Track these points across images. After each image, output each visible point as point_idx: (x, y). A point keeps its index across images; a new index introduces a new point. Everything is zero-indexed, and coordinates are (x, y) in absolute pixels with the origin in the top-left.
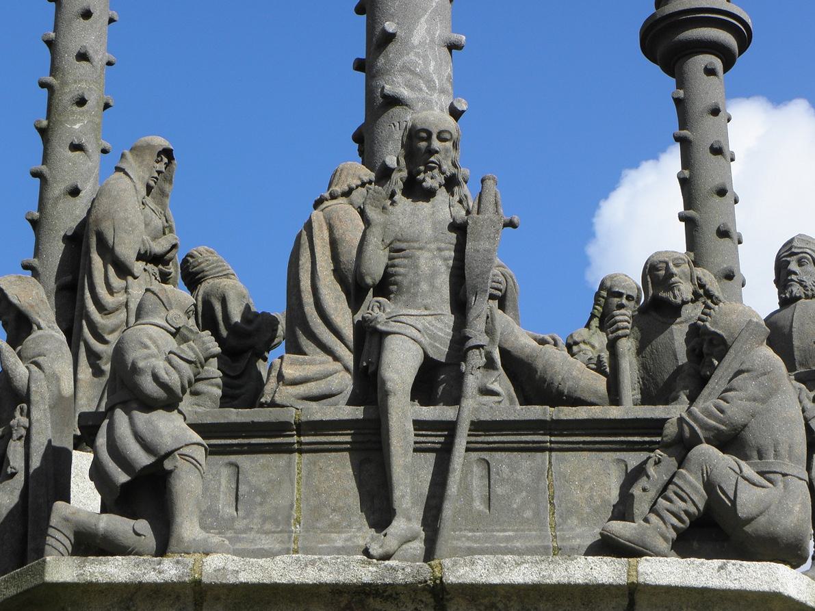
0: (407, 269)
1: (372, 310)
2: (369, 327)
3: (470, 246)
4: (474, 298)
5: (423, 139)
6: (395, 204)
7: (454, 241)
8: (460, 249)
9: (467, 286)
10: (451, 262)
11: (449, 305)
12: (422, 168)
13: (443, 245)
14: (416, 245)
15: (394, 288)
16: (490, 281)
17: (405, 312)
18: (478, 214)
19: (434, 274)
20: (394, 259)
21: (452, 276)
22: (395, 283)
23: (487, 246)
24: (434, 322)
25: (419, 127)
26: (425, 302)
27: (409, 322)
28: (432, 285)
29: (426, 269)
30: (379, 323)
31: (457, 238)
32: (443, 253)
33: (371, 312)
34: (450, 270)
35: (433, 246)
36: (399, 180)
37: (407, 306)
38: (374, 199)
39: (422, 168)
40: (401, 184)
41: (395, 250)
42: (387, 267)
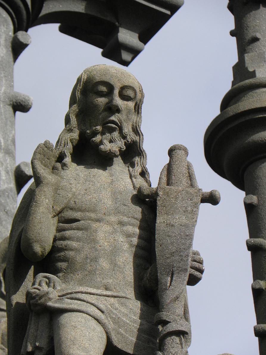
0: (81, 244)
2: (36, 305)
3: (160, 220)
4: (169, 279)
5: (101, 94)
6: (65, 168)
7: (139, 216)
8: (148, 227)
9: (158, 266)
11: (133, 289)
13: (125, 219)
14: (93, 215)
15: (62, 265)
16: (190, 259)
17: (82, 289)
19: (115, 251)
21: (136, 256)
23: (184, 220)
24: (117, 305)
25: (98, 79)
26: (105, 281)
27: (90, 300)
28: (114, 264)
29: (106, 244)
30: (50, 299)
31: (143, 212)
32: (125, 228)
34: (134, 249)
35: (113, 219)
36: (69, 141)
37: (81, 283)
39: (99, 128)
40: (70, 146)
41: (66, 220)
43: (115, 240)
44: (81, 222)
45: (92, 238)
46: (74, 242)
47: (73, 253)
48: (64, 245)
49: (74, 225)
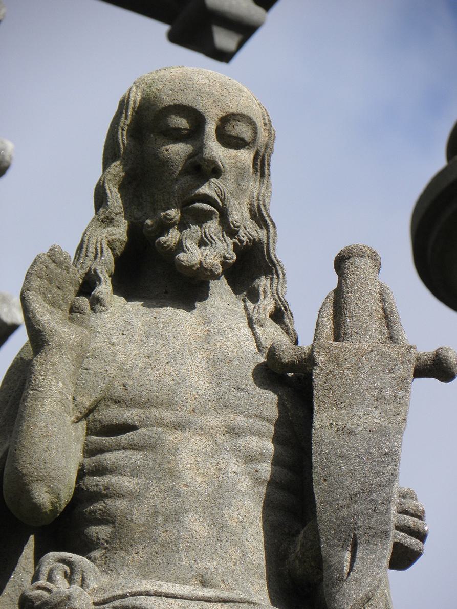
1: (50, 579)
3: (323, 421)
4: (348, 555)
5: (176, 136)
7: (273, 412)
9: (322, 527)
10: (266, 469)
11: (264, 582)
12: (174, 213)
13: (241, 421)
14: (166, 415)
15: (100, 532)
16: (394, 509)
18: (337, 337)
19: (220, 495)
20: (102, 450)
21: (269, 506)
22: (105, 519)
23: (376, 418)
25: (167, 101)
26: (200, 566)
29: (199, 479)
31: (281, 404)
32: (241, 442)
33: (49, 585)
34: (263, 490)
35: (214, 421)
36: (105, 247)
38: (50, 281)
41: (105, 428)
42: (82, 474)
43: (220, 470)
44: (139, 431)
45: (166, 466)
46: (125, 478)
47: (125, 502)
48: (103, 486)
49: (124, 438)
